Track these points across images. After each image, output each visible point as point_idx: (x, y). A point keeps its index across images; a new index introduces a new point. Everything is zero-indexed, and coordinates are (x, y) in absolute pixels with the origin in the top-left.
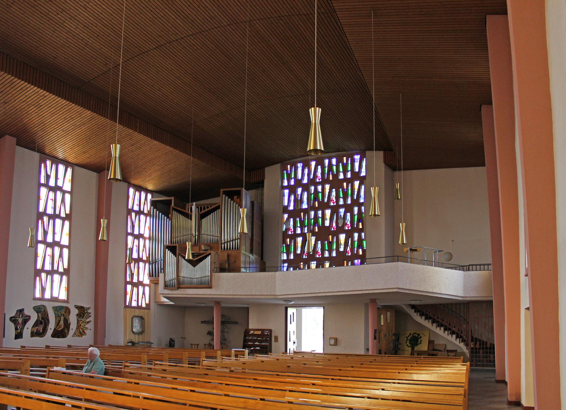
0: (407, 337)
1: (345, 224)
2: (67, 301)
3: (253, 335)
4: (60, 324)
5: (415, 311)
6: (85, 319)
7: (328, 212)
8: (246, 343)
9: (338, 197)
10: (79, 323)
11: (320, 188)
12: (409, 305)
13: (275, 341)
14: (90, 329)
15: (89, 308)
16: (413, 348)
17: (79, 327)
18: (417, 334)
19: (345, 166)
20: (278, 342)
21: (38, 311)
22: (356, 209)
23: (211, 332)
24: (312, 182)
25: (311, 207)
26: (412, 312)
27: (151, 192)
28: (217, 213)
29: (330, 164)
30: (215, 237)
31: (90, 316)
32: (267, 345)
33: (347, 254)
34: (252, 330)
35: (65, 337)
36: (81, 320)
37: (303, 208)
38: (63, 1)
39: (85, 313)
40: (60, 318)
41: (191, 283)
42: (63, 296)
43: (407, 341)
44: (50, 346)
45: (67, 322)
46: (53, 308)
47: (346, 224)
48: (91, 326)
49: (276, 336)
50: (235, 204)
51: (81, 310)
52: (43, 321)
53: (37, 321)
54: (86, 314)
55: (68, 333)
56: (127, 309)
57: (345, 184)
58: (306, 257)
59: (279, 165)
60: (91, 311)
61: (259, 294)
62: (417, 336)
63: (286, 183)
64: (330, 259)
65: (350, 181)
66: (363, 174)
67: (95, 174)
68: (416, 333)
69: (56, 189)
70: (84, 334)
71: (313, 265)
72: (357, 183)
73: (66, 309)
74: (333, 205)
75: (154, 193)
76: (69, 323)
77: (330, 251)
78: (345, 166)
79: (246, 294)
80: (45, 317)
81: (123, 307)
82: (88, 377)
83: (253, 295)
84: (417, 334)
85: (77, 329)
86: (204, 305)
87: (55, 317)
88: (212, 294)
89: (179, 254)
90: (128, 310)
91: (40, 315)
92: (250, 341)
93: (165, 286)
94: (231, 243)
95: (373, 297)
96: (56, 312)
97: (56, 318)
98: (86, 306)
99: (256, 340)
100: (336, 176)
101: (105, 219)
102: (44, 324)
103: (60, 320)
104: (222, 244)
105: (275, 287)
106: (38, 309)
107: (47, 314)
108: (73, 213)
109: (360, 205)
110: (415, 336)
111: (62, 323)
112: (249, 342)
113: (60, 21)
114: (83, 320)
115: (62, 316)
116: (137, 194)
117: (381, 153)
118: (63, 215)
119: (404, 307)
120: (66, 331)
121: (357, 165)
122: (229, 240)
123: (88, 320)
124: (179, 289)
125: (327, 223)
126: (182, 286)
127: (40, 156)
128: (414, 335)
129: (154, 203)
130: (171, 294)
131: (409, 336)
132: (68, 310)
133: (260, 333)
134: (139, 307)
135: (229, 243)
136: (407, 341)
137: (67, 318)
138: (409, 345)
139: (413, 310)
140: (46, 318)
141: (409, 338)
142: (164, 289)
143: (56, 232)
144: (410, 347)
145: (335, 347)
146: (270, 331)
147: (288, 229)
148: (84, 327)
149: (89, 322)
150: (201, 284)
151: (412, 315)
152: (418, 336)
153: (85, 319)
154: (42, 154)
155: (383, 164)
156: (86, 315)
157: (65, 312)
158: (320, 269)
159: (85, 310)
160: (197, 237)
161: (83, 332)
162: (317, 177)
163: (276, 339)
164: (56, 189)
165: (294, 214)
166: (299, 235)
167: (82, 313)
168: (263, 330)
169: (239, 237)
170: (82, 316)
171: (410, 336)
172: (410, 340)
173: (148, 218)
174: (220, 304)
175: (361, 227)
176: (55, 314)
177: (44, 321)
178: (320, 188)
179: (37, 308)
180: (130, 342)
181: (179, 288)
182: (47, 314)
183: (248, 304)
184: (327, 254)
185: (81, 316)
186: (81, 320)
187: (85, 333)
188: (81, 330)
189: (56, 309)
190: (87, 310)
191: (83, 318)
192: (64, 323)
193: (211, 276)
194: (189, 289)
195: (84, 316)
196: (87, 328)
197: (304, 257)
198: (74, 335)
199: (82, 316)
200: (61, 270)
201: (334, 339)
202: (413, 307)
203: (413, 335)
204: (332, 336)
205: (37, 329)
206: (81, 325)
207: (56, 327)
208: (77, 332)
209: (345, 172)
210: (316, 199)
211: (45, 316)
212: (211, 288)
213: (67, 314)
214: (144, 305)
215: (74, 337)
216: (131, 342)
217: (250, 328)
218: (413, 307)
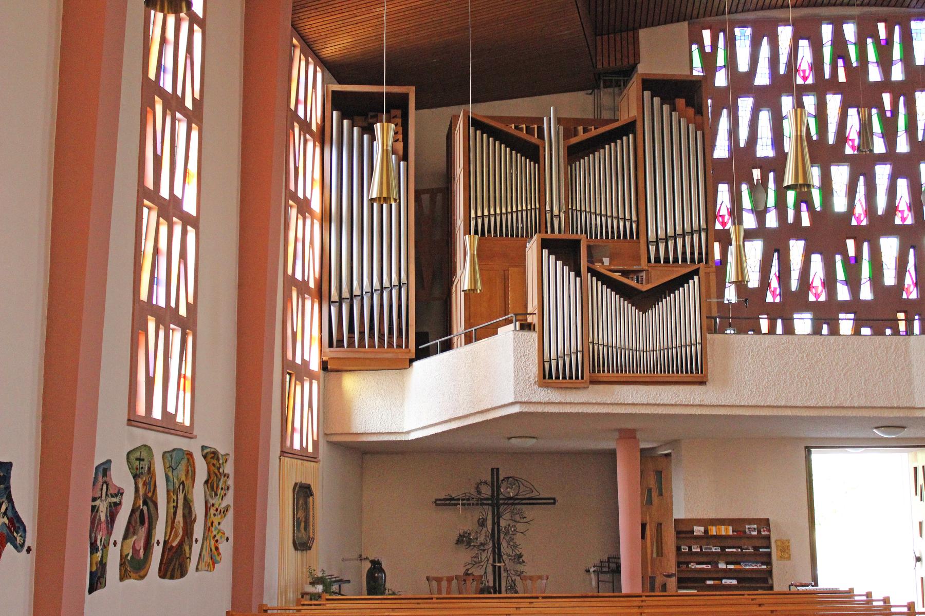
1: (892, 207)
3: (706, 536)
7: (840, 174)
14: (227, 539)
19: (884, 51)
20: (789, 558)
28: (624, 145)
29: (839, 40)
30: (621, 223)
33: (905, 296)
34: (699, 522)
39: (220, 474)
41: (633, 366)
49: (784, 538)
51: (214, 465)
57: (887, 98)
58: (778, 300)
59: (685, 25)
64: (854, 306)
71: (803, 323)
73: (188, 460)
76: (193, 517)
77: (853, 283)
78: (884, 51)
79: (820, 404)
83: (843, 407)
86: (530, 443)
94: (696, 237)
95: (629, 425)
98: (222, 451)
100: (858, 73)
101: (388, 121)
114: (216, 501)
120: (187, 548)
122: (687, 228)
123: (224, 504)
135: (671, 244)
142: (541, 385)
149: (227, 509)
158: (878, 338)
161: (217, 549)
163: (785, 549)
174: (635, 438)
184: (843, 293)
197: (769, 299)
209: (885, 63)
212: (703, 383)
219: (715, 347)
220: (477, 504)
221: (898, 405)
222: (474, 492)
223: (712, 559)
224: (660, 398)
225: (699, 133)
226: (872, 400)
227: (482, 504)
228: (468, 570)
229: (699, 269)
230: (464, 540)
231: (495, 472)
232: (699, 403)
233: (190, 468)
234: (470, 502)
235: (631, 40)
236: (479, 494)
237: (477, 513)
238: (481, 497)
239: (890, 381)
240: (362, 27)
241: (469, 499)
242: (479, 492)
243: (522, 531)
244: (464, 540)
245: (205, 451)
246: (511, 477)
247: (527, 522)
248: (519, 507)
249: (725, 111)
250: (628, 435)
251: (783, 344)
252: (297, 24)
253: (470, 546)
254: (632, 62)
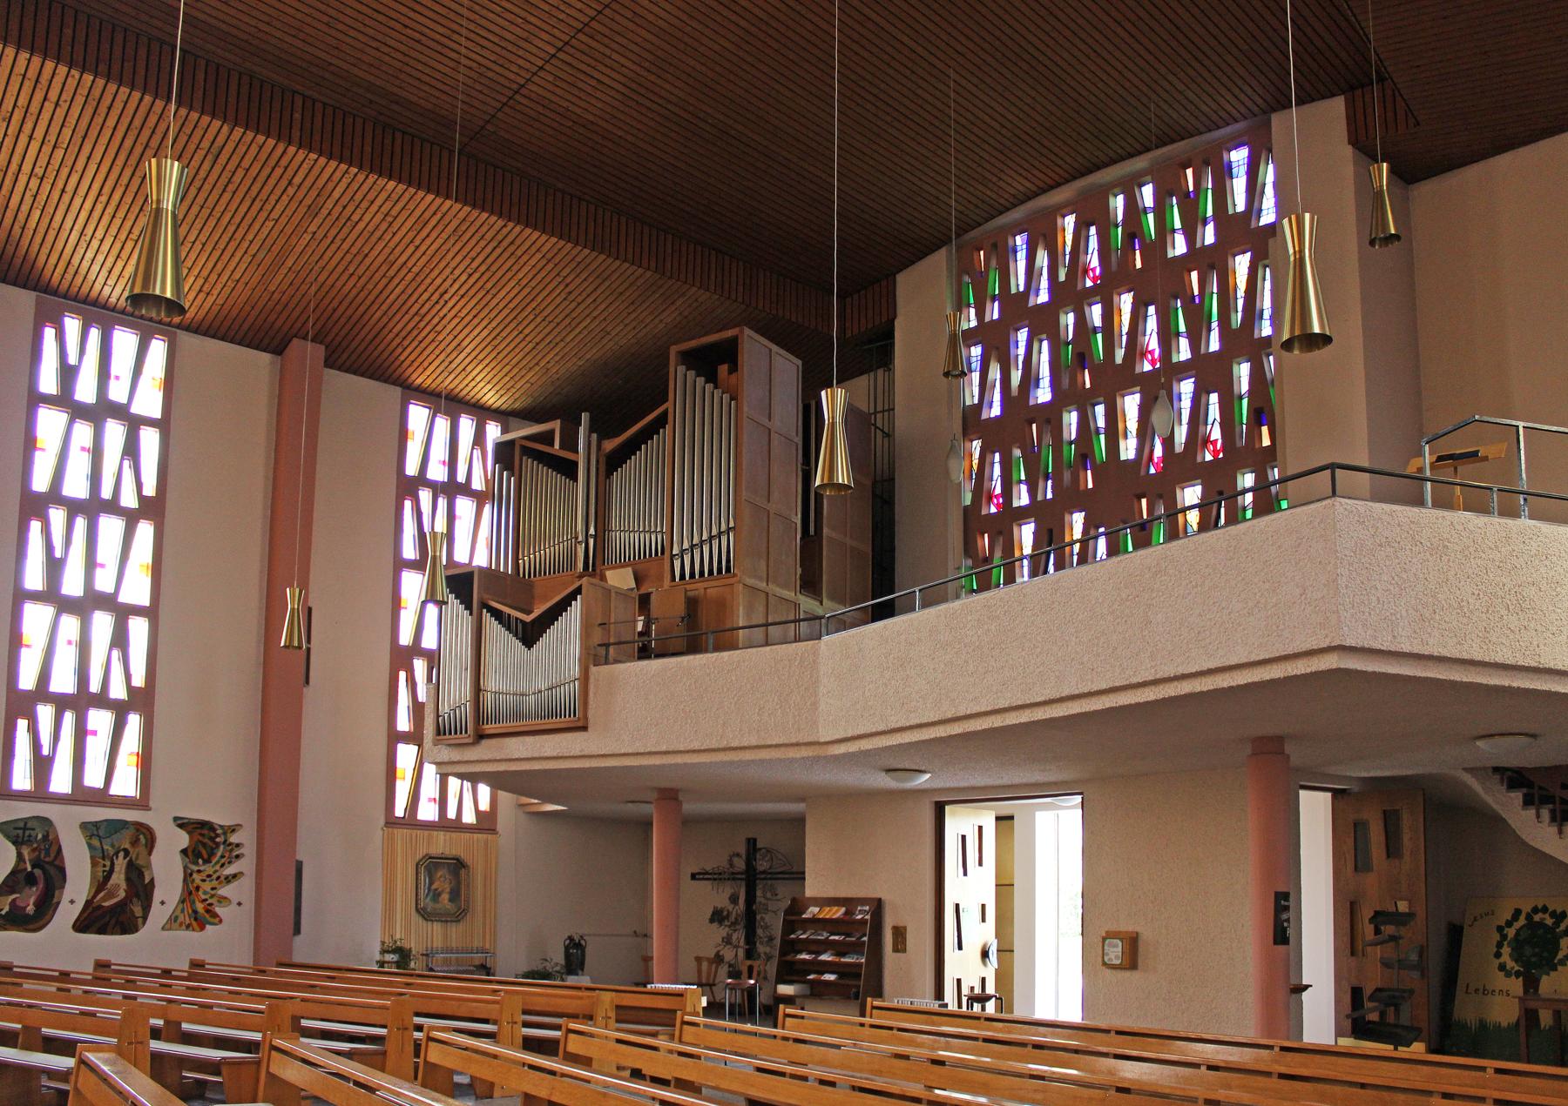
0: (1500, 929)
1: (1197, 438)
2: (141, 803)
3: (815, 921)
4: (111, 882)
5: (1528, 802)
6: (217, 867)
7: (1131, 404)
8: (789, 958)
9: (1167, 336)
10: (193, 880)
12: (1496, 770)
13: (896, 950)
14: (239, 904)
15: (233, 829)
16: (1531, 984)
17: (190, 893)
18: (1553, 914)
21: (18, 836)
22: (1243, 371)
23: (721, 911)
24: (1068, 294)
25: (1063, 397)
26: (1510, 806)
27: (501, 415)
29: (1133, 209)
31: (237, 857)
32: (860, 965)
35: (137, 931)
36: (199, 871)
40: (113, 864)
41: (518, 715)
42: (126, 783)
43: (1500, 945)
44: (113, 961)
45: (141, 875)
46: (84, 826)
47: (1207, 441)
48: (240, 892)
49: (901, 924)
50: (717, 393)
52: (38, 872)
53: (13, 873)
54: (222, 847)
55: (145, 918)
56: (395, 831)
59: (940, 259)
60: (245, 838)
62: (1549, 922)
65: (1213, 261)
66: (1268, 217)
67: (265, 358)
68: (1545, 909)
69: (101, 411)
72: (1242, 264)
73: (138, 830)
74: (1151, 368)
76: (147, 881)
80: (47, 859)
81: (382, 822)
82: (676, 1055)
84: (1553, 914)
85: (182, 901)
87: (92, 858)
89: (484, 605)
90: (400, 833)
91: (26, 852)
92: (808, 946)
93: (438, 733)
94: (706, 549)
96: (96, 842)
97: (94, 864)
98: (219, 818)
99: (826, 946)
102: (41, 886)
103: (112, 870)
104: (672, 557)
105: (815, 705)
106: (20, 832)
107: (54, 848)
108: (171, 497)
109: (1257, 350)
110: (1541, 924)
111: (119, 878)
112: (800, 952)
113: (480, 32)
114: (208, 869)
115: (121, 854)
117: (1335, 108)
118: (129, 500)
119: (1468, 779)
121: (1239, 185)
123: (229, 870)
124: (484, 742)
125: (1128, 450)
126: (486, 726)
127: (38, 303)
128: (1537, 918)
130: (459, 762)
131: (1509, 924)
132: (145, 836)
133: (838, 912)
134: (445, 824)
136: (1500, 945)
137: (140, 862)
138: (1510, 964)
139: (1517, 797)
140: (51, 863)
141: (1511, 932)
143: (99, 560)
144: (1518, 974)
145: (1127, 974)
146: (878, 906)
147: (981, 492)
148: (212, 896)
149: (235, 876)
150: (552, 714)
151: (1514, 822)
152: (1557, 924)
153: (217, 867)
154: (45, 292)
155: (1348, 151)
156: (219, 854)
157: (135, 842)
159: (218, 836)
160: (591, 541)
162: (1086, 271)
164: (101, 411)
165: (997, 436)
167: (204, 845)
170: (206, 856)
171: (1517, 925)
172: (1518, 946)
174: (676, 799)
175: (1266, 442)
176: (90, 846)
177: (45, 872)
178: (1096, 313)
179: (16, 828)
180: (394, 951)
181: (480, 736)
182: (54, 848)
183: (802, 800)
185: (198, 855)
186: (199, 871)
187: (215, 915)
188: (200, 907)
189: (91, 830)
190: (225, 833)
191: (207, 861)
192: (128, 879)
193: (585, 678)
195: (212, 854)
196: (223, 900)
198: (172, 923)
199: (206, 856)
200: (118, 691)
201: (1122, 940)
202: (1516, 778)
203: (1529, 917)
204: (1114, 927)
205: (14, 900)
206: (198, 888)
207: (94, 896)
208: (183, 911)
210: (1082, 359)
211: (48, 854)
212: (584, 728)
213: (142, 850)
214: (469, 817)
215: (170, 929)
216: (397, 950)
217: (809, 893)
218: (1516, 778)
223: (818, 947)
227: (734, 879)
228: (719, 951)
230: (718, 917)
231: (752, 843)
232: (579, 754)
233: (141, 837)
237: (727, 890)
240: (341, 268)
242: (731, 865)
244: (718, 917)
245: (179, 822)
248: (769, 882)
249: (1152, 310)
250: (669, 796)
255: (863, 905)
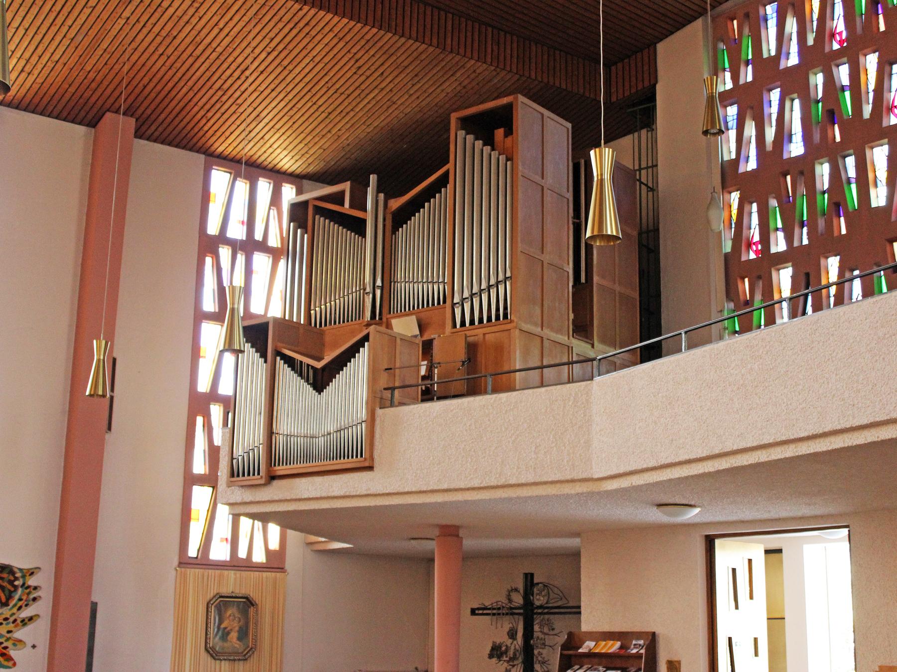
6: (15, 610)
11: (843, 74)
23: (500, 647)
27: (296, 178)
31: (34, 599)
37: (793, 155)
38: (647, 2)
39: (16, 587)
41: (308, 456)
54: (20, 591)
60: (43, 581)
61: (531, 478)
63: (727, 83)
67: (81, 130)
70: (6, 663)
75: (305, 182)
81: (176, 562)
88: (372, 491)
90: (192, 572)
93: (232, 475)
104: (453, 305)
116: (242, 187)
123: (25, 613)
124: (276, 483)
126: (277, 468)
129: (299, 213)
133: (614, 647)
134: (236, 564)
146: (652, 640)
147: (740, 240)
148: (8, 639)
149: (31, 619)
153: (15, 610)
156: (17, 597)
159: (16, 579)
160: (378, 292)
162: (833, 35)
166: (780, 260)
168: (624, 637)
169: (508, 274)
173: (282, 263)
174: (457, 536)
178: (843, 74)
181: (272, 477)
183: (577, 535)
190: (24, 577)
193: (372, 420)
194: (304, 480)
195: (10, 597)
196: (18, 642)
210: (832, 116)
212: (370, 468)
214: (259, 557)
217: (585, 627)
219: (385, 424)
220: (507, 614)
221: (572, 476)
222: (505, 600)
224: (331, 490)
225: (509, 163)
226: (543, 473)
227: (513, 614)
229: (369, 333)
231: (529, 578)
232: (365, 493)
234: (500, 611)
235: (646, 59)
236: (510, 602)
237: (506, 624)
238: (512, 606)
239: (564, 445)
241: (499, 609)
242: (510, 601)
243: (551, 644)
246: (541, 583)
247: (555, 635)
248: (547, 617)
251: (452, 411)
252: (212, 145)
253: (500, 661)
254: (646, 84)
255: (638, 639)
